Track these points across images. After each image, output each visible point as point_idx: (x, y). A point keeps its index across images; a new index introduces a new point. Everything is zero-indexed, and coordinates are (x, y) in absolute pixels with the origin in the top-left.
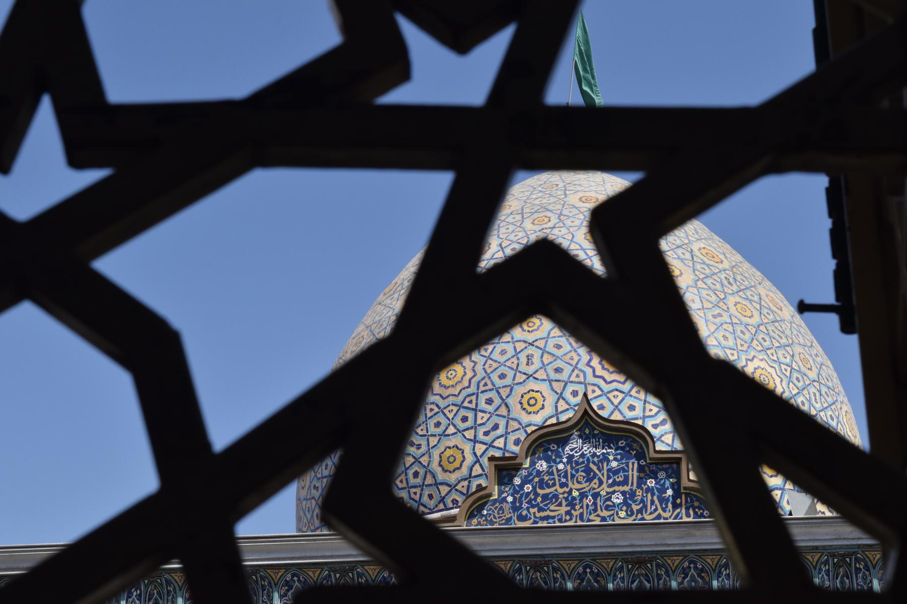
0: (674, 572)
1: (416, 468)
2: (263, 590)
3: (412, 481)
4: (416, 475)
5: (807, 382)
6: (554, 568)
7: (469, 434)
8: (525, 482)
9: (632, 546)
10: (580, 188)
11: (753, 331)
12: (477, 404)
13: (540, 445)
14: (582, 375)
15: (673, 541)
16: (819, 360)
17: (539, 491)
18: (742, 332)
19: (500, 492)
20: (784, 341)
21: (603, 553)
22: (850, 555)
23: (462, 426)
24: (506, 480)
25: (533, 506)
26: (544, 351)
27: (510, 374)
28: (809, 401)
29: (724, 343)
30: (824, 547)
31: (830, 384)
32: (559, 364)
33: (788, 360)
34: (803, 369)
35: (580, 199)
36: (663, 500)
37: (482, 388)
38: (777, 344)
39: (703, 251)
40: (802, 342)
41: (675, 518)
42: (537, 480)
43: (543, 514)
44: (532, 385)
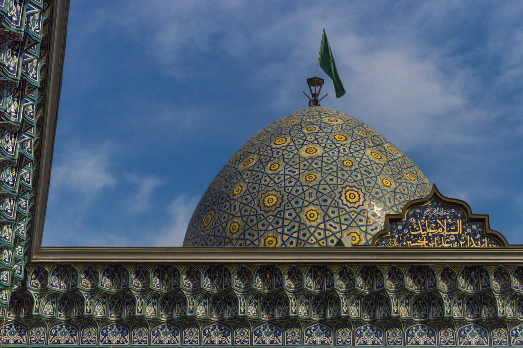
8: (404, 227)
12: (284, 216)
14: (336, 204)
26: (318, 191)
35: (329, 120)
37: (286, 208)
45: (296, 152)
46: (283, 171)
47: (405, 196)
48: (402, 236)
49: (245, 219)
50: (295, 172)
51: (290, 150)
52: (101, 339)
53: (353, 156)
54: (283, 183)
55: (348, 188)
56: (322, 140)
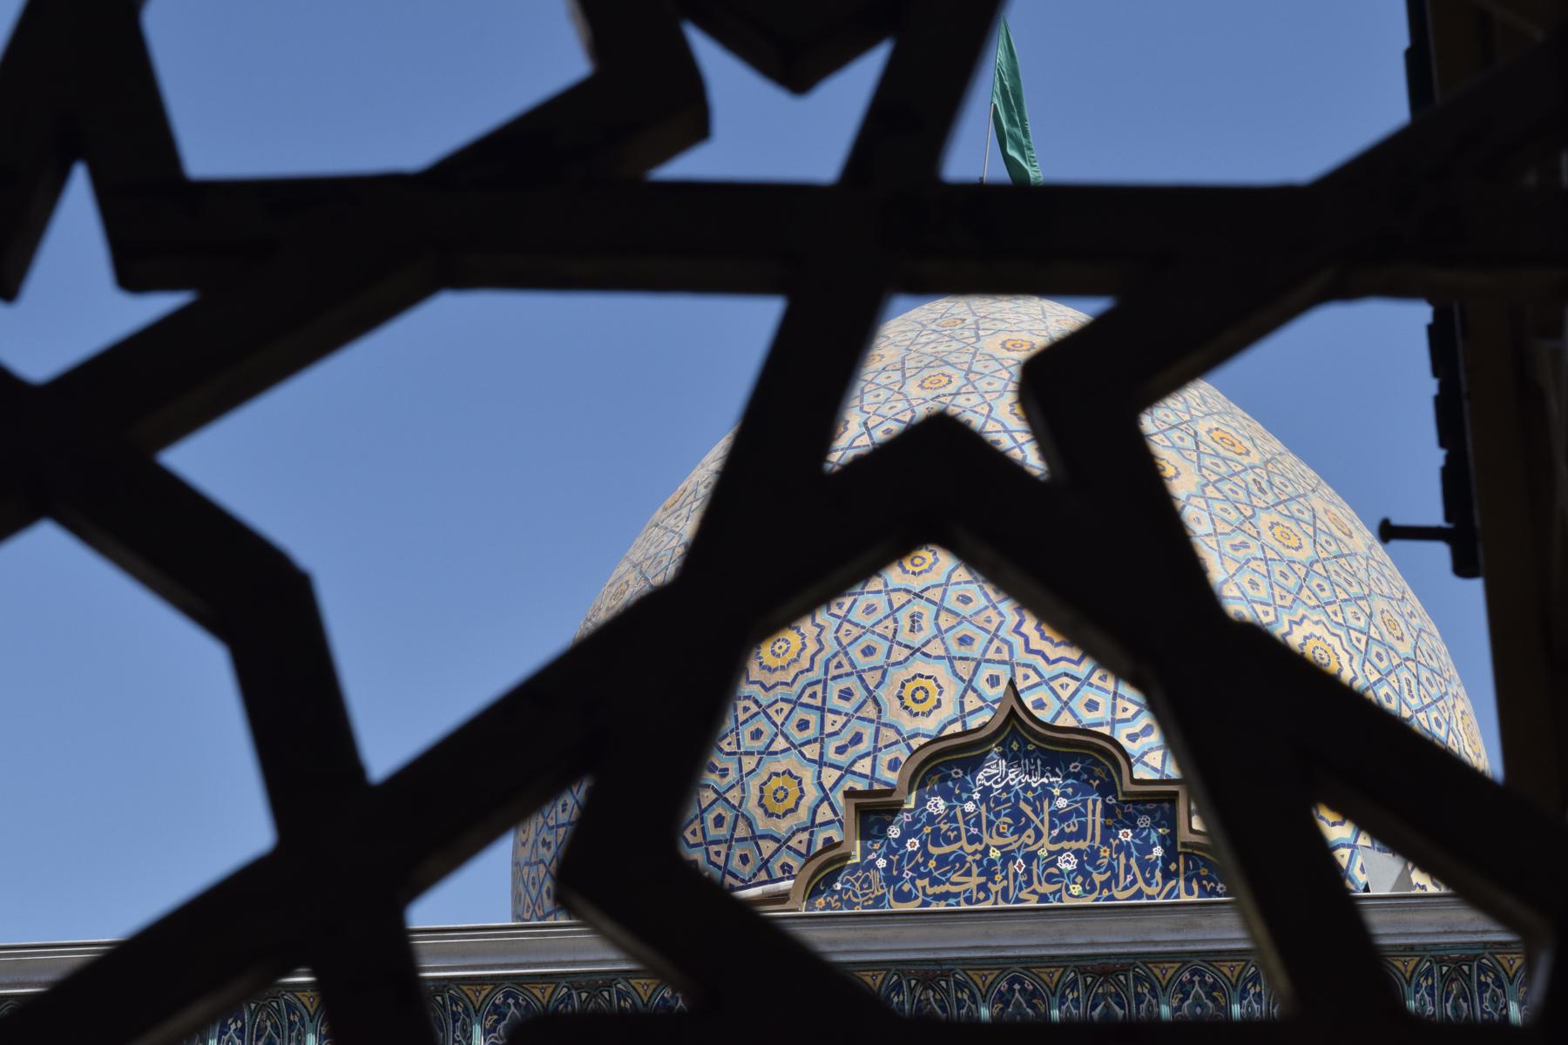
0: (1164, 990)
1: (719, 809)
2: (455, 1021)
3: (713, 832)
4: (719, 821)
5: (1396, 661)
6: (957, 983)
7: (812, 751)
8: (907, 833)
9: (1092, 944)
10: (1002, 326)
11: (1302, 573)
12: (824, 699)
13: (934, 771)
14: (1005, 649)
15: (1163, 935)
16: (1416, 622)
17: (931, 849)
18: (1283, 575)
19: (865, 852)
20: (1355, 590)
21: (1042, 957)
22: (1469, 960)
23: (799, 737)
24: (875, 831)
25: (922, 876)
26: (940, 608)
27: (882, 647)
28: (1399, 694)
29: (1251, 593)
30: (1425, 947)
31: (1434, 664)
32: (966, 629)
33: (1362, 624)
34: (1389, 639)
35: (1003, 345)
36: (1146, 866)
37: (833, 672)
38: (1343, 596)
39: (1215, 434)
40: (1386, 591)
41: (1168, 896)
42: (928, 830)
43: (938, 889)
44: (919, 665)
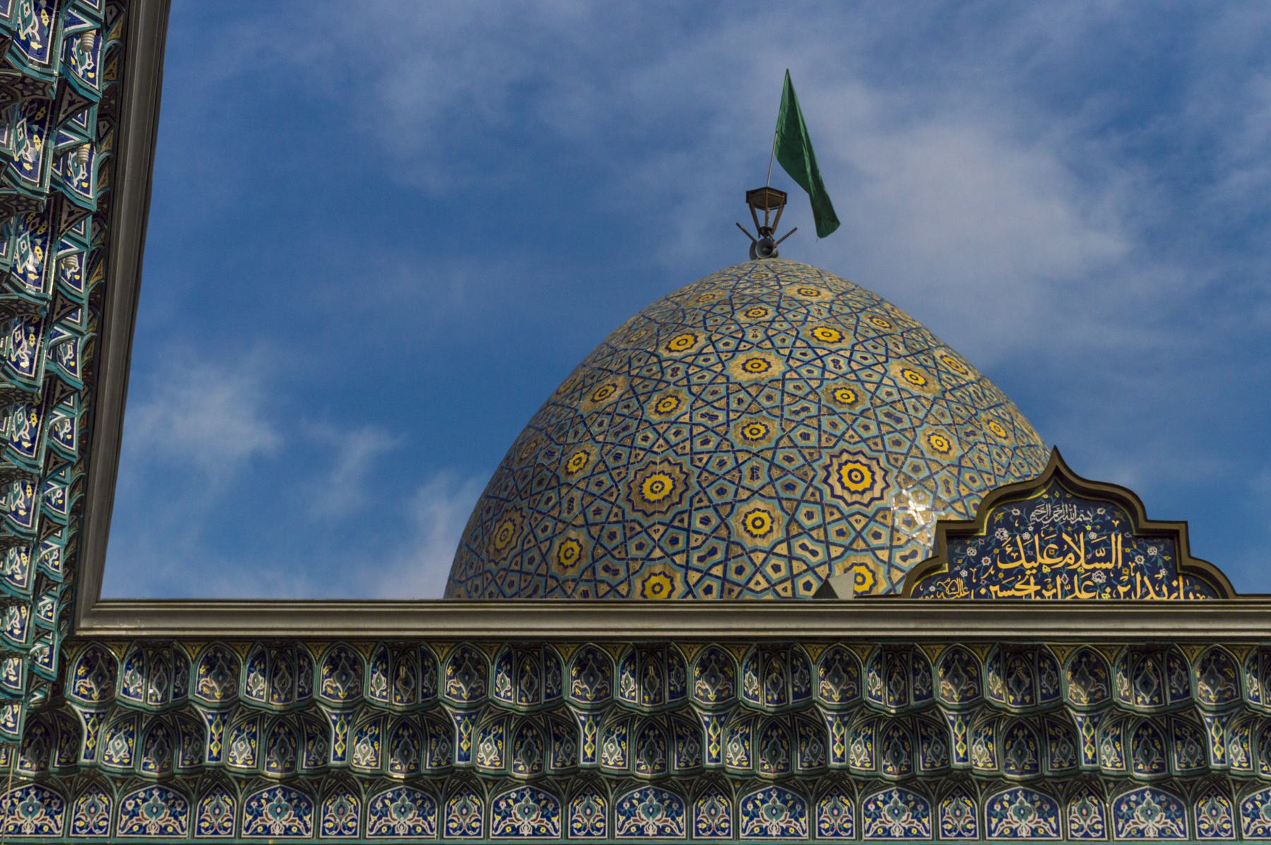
8: (982, 552)
12: (689, 523)
14: (818, 494)
26: (772, 464)
35: (799, 291)
37: (696, 505)
45: (718, 368)
46: (687, 416)
47: (985, 476)
48: (977, 573)
49: (595, 531)
50: (716, 417)
51: (705, 364)
52: (245, 824)
53: (859, 380)
54: (687, 444)
55: (845, 457)
56: (783, 340)
